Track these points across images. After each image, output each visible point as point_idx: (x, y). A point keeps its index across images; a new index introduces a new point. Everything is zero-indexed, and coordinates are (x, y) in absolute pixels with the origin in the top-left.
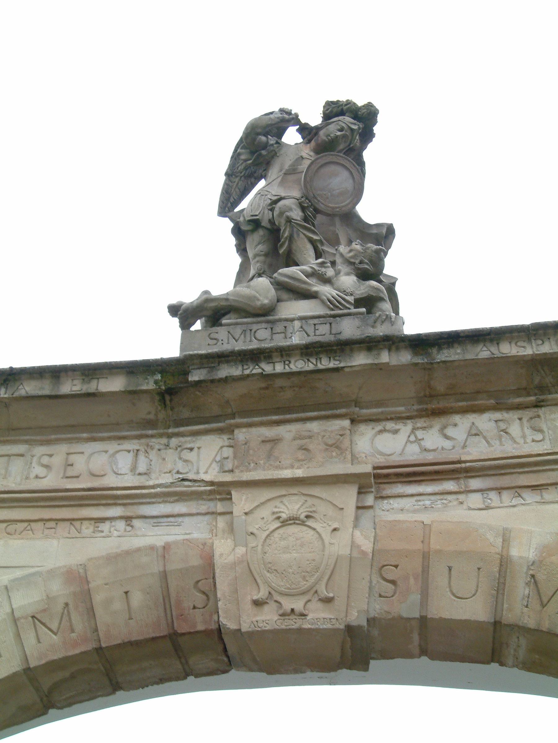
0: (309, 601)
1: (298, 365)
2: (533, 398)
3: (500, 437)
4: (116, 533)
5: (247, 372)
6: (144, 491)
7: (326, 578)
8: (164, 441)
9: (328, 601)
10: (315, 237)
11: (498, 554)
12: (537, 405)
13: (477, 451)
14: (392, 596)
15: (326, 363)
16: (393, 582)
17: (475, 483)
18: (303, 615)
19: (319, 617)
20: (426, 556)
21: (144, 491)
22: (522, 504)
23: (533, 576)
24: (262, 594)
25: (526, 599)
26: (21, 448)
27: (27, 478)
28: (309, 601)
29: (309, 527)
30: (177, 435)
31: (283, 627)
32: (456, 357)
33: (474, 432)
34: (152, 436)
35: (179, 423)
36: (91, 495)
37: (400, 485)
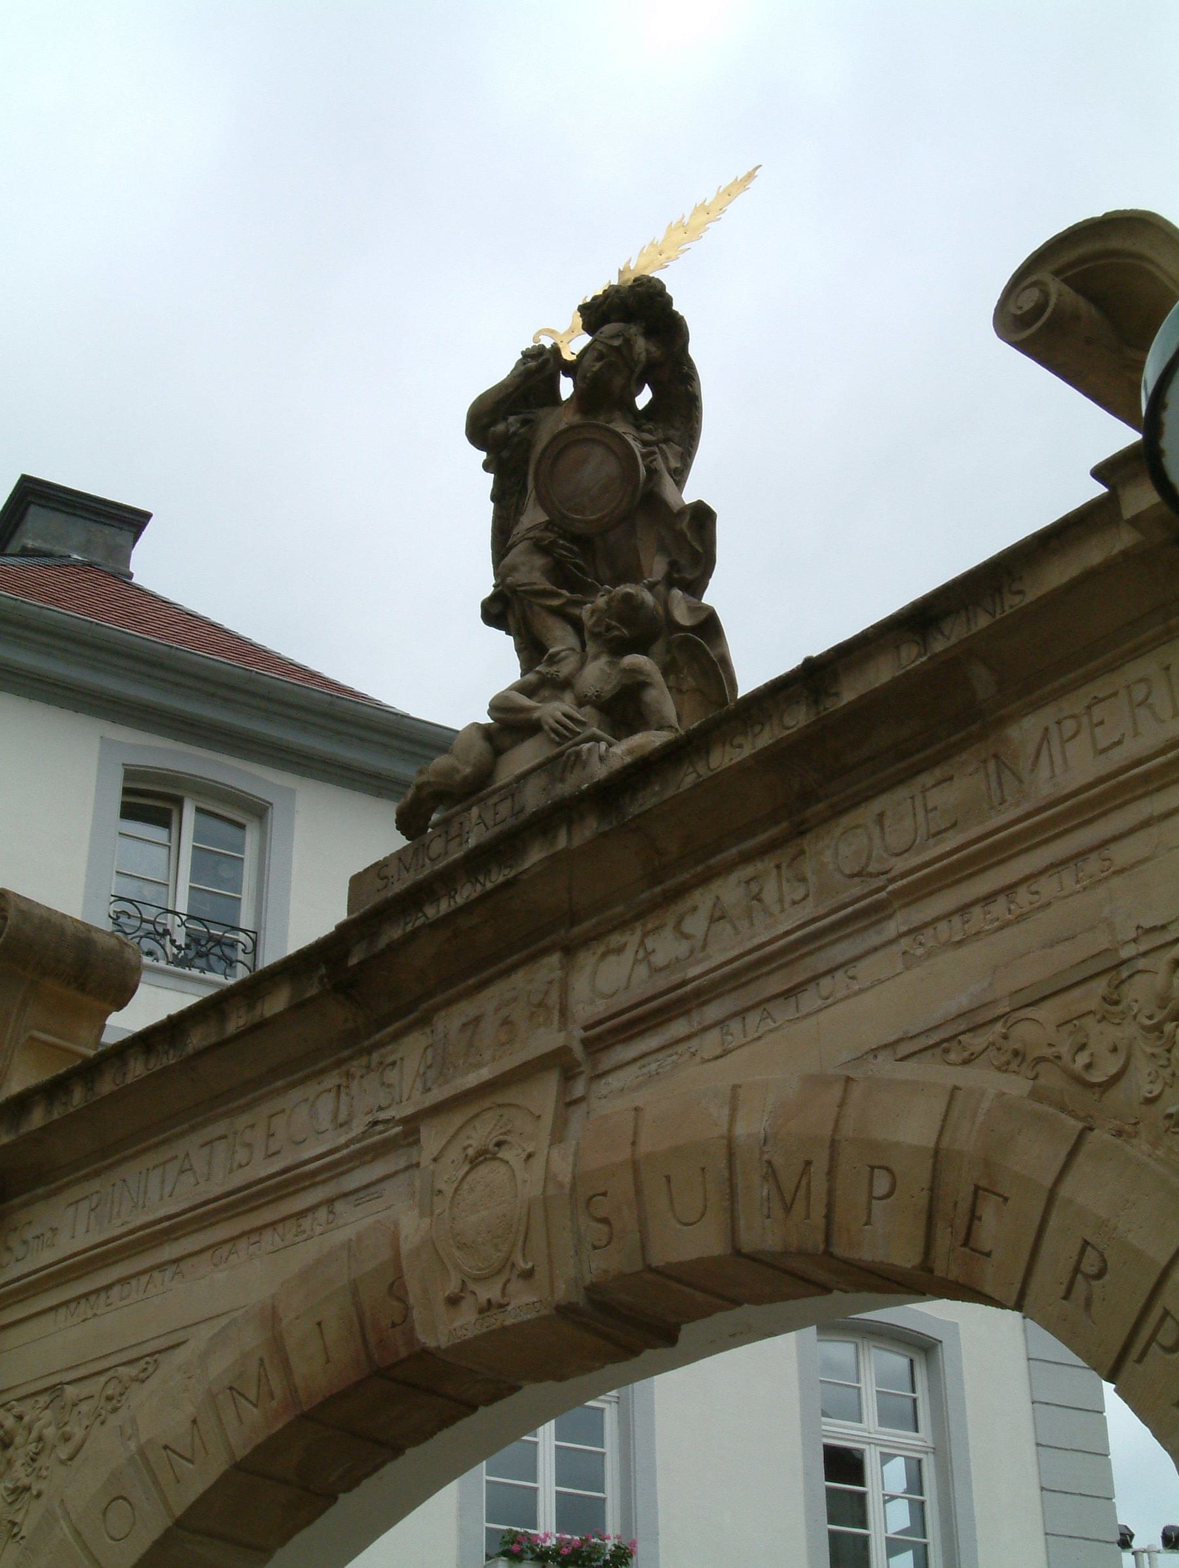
0: (508, 1281)
1: (466, 893)
2: (785, 825)
3: (749, 913)
4: (318, 1229)
5: (409, 928)
6: (337, 1156)
7: (520, 1243)
8: (364, 1060)
9: (528, 1275)
10: (556, 602)
11: (723, 1137)
12: (800, 831)
13: (726, 948)
14: (609, 1243)
15: (498, 877)
16: (605, 1221)
17: (713, 1012)
18: (501, 1306)
19: (524, 1303)
20: (635, 1166)
21: (337, 1156)
22: (771, 1031)
23: (769, 1163)
24: (453, 1287)
25: (766, 1204)
26: (219, 1128)
27: (231, 1171)
28: (508, 1281)
29: (501, 1160)
30: (380, 1045)
31: (485, 1330)
32: (654, 801)
33: (717, 914)
34: (351, 1058)
35: (382, 1024)
36: (285, 1180)
37: (619, 1048)
